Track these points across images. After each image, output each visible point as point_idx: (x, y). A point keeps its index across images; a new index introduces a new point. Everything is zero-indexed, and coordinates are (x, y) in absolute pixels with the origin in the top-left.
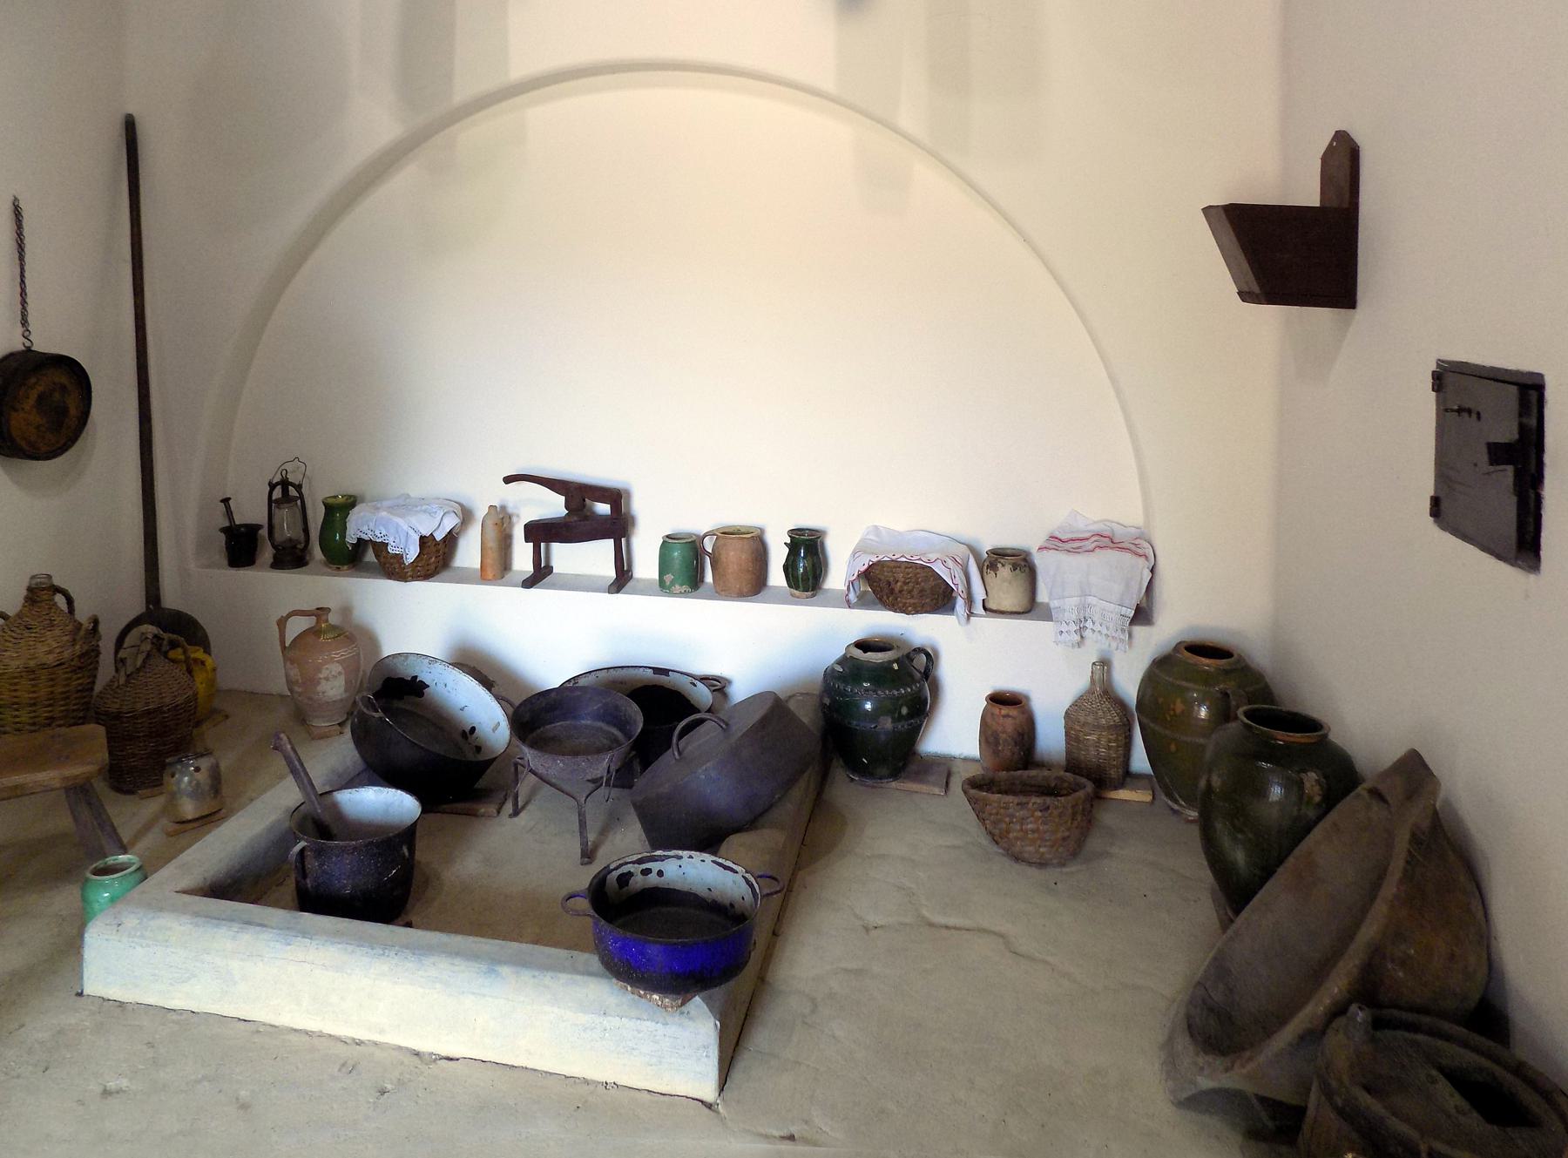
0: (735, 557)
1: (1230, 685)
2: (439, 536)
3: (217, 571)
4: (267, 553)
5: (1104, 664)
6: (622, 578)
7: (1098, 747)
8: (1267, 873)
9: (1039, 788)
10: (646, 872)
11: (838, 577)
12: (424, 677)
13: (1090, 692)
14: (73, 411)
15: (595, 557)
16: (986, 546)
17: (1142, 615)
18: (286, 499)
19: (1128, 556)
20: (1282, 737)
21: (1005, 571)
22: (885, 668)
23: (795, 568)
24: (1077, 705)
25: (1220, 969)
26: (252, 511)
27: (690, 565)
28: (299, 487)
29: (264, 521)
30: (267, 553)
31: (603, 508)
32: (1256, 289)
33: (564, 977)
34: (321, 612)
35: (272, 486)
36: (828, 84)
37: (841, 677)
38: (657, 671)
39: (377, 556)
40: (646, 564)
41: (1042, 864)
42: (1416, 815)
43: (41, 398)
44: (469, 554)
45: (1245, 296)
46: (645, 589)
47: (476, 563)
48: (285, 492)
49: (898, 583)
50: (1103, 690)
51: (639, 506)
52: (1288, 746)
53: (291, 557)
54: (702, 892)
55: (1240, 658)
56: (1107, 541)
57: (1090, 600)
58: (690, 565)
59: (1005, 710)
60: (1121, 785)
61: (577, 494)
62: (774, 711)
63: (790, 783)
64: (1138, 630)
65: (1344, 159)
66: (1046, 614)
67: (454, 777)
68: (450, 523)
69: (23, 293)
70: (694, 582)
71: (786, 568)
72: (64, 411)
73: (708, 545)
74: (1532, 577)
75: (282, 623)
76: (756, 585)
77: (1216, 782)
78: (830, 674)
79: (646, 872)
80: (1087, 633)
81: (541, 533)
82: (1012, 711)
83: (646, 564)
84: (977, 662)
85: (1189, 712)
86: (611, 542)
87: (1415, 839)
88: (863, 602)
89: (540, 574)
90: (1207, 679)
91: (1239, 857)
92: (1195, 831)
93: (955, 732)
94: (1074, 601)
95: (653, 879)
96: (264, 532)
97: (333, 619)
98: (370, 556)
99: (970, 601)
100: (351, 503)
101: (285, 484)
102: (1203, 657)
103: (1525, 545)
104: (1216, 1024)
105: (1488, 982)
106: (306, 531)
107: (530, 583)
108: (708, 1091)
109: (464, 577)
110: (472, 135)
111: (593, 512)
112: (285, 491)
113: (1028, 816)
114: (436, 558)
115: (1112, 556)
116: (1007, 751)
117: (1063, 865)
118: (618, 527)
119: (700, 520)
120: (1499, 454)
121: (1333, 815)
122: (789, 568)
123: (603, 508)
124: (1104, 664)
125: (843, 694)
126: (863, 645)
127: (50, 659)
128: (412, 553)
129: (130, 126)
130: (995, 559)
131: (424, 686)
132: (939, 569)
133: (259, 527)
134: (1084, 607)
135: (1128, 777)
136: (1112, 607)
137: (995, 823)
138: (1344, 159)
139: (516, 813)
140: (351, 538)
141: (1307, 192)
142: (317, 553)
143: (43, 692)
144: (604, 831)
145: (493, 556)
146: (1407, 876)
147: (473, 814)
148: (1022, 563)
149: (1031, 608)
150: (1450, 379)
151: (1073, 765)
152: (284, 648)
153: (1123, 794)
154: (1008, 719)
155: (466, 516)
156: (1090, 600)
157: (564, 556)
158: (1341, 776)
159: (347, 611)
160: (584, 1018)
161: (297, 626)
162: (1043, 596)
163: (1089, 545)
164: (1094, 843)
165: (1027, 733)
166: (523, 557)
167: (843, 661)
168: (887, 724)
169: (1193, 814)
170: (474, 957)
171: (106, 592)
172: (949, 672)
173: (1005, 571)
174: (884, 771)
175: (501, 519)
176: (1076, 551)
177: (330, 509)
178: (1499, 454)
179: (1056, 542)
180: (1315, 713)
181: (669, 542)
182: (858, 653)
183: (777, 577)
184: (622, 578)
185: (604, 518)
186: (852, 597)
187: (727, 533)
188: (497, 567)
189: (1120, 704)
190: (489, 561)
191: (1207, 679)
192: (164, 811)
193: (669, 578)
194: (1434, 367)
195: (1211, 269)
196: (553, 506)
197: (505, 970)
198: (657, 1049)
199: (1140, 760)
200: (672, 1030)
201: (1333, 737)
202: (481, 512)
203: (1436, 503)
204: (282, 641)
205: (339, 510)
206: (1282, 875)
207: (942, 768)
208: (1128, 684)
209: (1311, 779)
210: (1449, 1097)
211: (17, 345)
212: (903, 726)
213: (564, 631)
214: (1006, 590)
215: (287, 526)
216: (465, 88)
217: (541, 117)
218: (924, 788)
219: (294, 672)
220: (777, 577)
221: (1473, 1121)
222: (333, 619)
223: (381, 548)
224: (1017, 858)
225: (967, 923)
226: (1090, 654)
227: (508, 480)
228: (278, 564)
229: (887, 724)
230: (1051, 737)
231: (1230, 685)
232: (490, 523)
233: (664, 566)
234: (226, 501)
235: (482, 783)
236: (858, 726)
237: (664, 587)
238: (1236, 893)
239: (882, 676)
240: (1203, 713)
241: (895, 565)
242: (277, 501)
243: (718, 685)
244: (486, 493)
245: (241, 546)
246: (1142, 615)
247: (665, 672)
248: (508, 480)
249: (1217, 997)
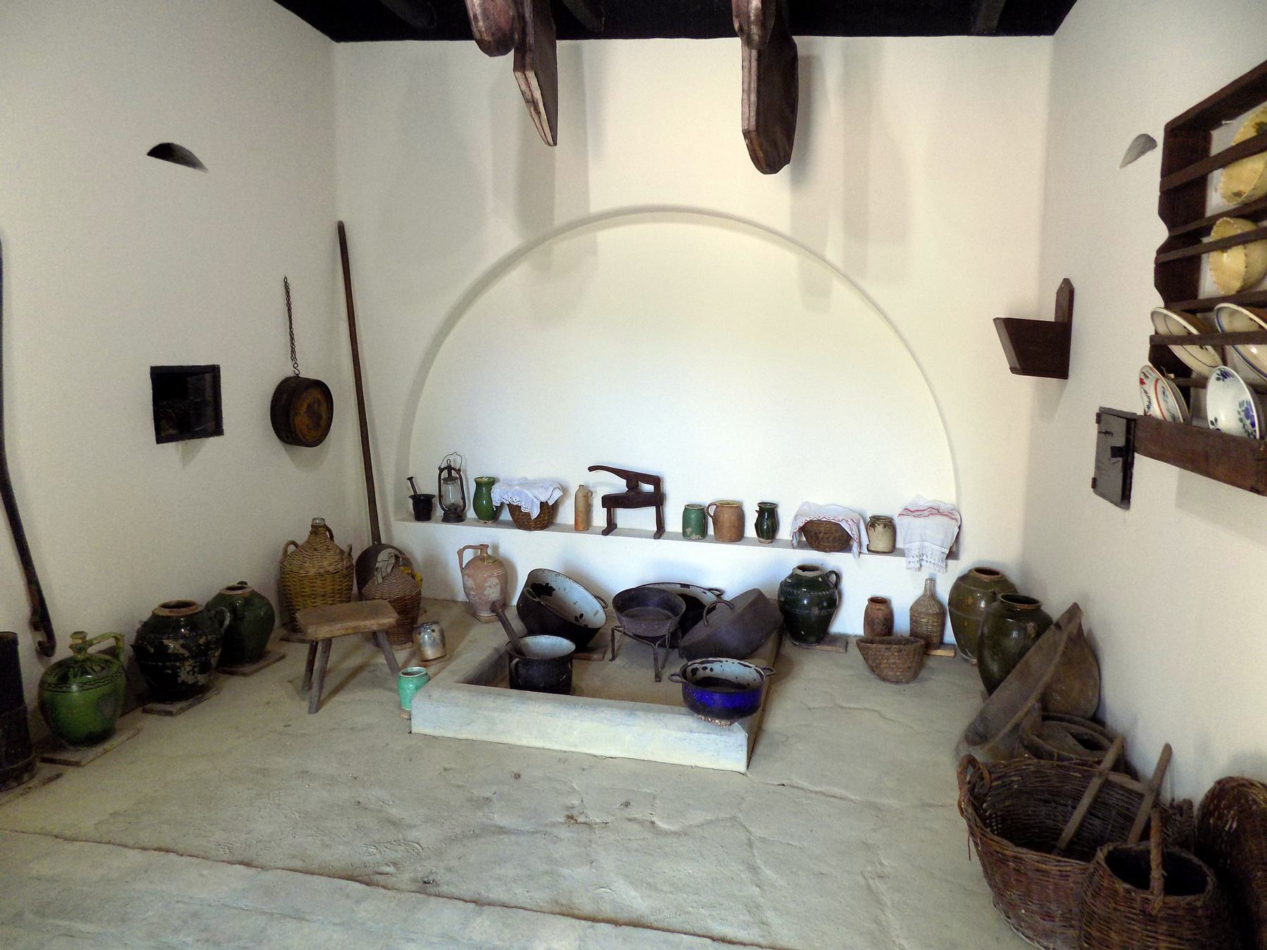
0: (727, 517)
1: (997, 589)
2: (551, 503)
3: (407, 523)
4: (439, 512)
5: (932, 581)
6: (660, 531)
7: (927, 624)
8: (1008, 673)
9: (895, 647)
10: (705, 668)
11: (786, 530)
12: (553, 584)
13: (924, 595)
14: (324, 416)
15: (644, 517)
16: (869, 515)
17: (952, 554)
18: (450, 479)
19: (946, 519)
20: (1019, 607)
21: (880, 528)
22: (814, 580)
23: (762, 526)
24: (917, 603)
25: (982, 717)
26: (428, 486)
27: (699, 523)
28: (458, 471)
29: (436, 492)
30: (439, 512)
31: (648, 488)
32: (1018, 366)
33: (669, 716)
34: (483, 547)
35: (441, 470)
36: (784, 226)
37: (791, 585)
38: (683, 585)
39: (512, 515)
40: (674, 522)
41: (898, 682)
42: (1072, 628)
43: (310, 406)
44: (567, 515)
45: (1013, 370)
46: (674, 537)
47: (572, 522)
48: (450, 474)
49: (822, 534)
50: (930, 594)
51: (668, 487)
52: (1022, 612)
53: (455, 515)
54: (734, 680)
55: (1003, 576)
56: (935, 511)
57: (926, 544)
58: (699, 523)
59: (878, 606)
60: (938, 648)
61: (633, 478)
62: (755, 600)
63: (768, 635)
64: (950, 562)
65: (1067, 294)
66: (902, 553)
67: (584, 637)
68: (557, 494)
69: (291, 334)
70: (703, 533)
71: (756, 525)
72: (320, 417)
73: (712, 511)
74: (1127, 513)
75: (460, 553)
76: (737, 536)
77: (986, 630)
78: (784, 585)
79: (705, 668)
80: (924, 563)
81: (611, 502)
82: (882, 607)
83: (674, 522)
84: (863, 580)
85: (976, 604)
86: (652, 510)
87: (1070, 638)
88: (800, 546)
89: (611, 528)
90: (985, 586)
91: (995, 668)
92: (976, 670)
93: (850, 620)
94: (917, 544)
95: (708, 672)
96: (436, 501)
97: (490, 552)
98: (506, 515)
99: (860, 545)
100: (492, 482)
101: (449, 468)
102: (984, 579)
103: (1124, 498)
104: (977, 735)
105: (1097, 708)
106: (463, 498)
107: (606, 532)
108: (742, 767)
109: (564, 529)
110: (563, 248)
111: (641, 491)
112: (450, 473)
113: (891, 658)
114: (546, 517)
115: (939, 519)
116: (878, 628)
117: (908, 682)
118: (657, 500)
119: (705, 498)
120: (1116, 452)
121: (1040, 641)
122: (758, 526)
123: (648, 488)
124: (932, 581)
125: (792, 594)
126: (802, 568)
127: (331, 569)
128: (535, 512)
129: (341, 229)
130: (874, 522)
131: (552, 589)
132: (844, 525)
133: (433, 496)
134: (922, 548)
135: (941, 644)
136: (937, 550)
137: (874, 660)
138: (1067, 294)
139: (613, 659)
140: (496, 502)
141: (1048, 314)
142: (471, 513)
143: (329, 589)
144: (663, 667)
145: (582, 516)
146: (1064, 654)
147: (589, 659)
148: (889, 524)
149: (892, 550)
150: (1104, 417)
151: (914, 633)
152: (462, 569)
153: (939, 652)
154: (880, 613)
155: (565, 490)
156: (926, 544)
157: (624, 516)
158: (1044, 623)
159: (496, 548)
160: (680, 734)
161: (468, 556)
162: (899, 545)
163: (926, 513)
164: (923, 674)
165: (889, 620)
166: (599, 516)
167: (791, 576)
168: (815, 611)
169: (975, 661)
170: (624, 708)
171: (351, 532)
172: (846, 585)
173: (880, 528)
174: (813, 639)
175: (585, 495)
176: (919, 516)
177: (479, 484)
178: (1116, 452)
179: (908, 512)
180: (1035, 596)
181: (687, 510)
182: (800, 572)
183: (750, 531)
184: (660, 531)
185: (648, 495)
186: (795, 542)
187: (721, 506)
188: (583, 523)
189: (941, 605)
190: (580, 519)
191: (985, 586)
192: (413, 655)
193: (689, 530)
194: (1097, 411)
195: (996, 353)
196: (620, 485)
197: (639, 713)
198: (715, 748)
199: (949, 636)
200: (725, 738)
201: (1042, 608)
202: (573, 490)
203: (1094, 480)
204: (461, 564)
205: (485, 485)
206: (1014, 673)
207: (843, 640)
208: (944, 593)
209: (1031, 626)
210: (1072, 741)
211: (289, 372)
212: (824, 612)
213: (628, 559)
214: (880, 534)
215: (452, 495)
216: (562, 216)
217: (606, 237)
218: (834, 648)
219: (470, 583)
220: (750, 531)
221: (1080, 748)
222: (490, 552)
223: (514, 509)
224: (884, 679)
225: (859, 706)
226: (925, 575)
227: (591, 469)
228: (446, 519)
229: (815, 611)
230: (902, 623)
231: (997, 589)
232: (580, 495)
233: (686, 523)
234: (410, 479)
235: (590, 645)
236: (797, 614)
237: (685, 535)
238: (991, 684)
239: (812, 584)
240: (983, 605)
241: (820, 522)
242: (445, 479)
243: (719, 593)
244: (577, 477)
245: (423, 508)
246: (952, 554)
247: (687, 586)
248: (591, 469)
249: (981, 729)
